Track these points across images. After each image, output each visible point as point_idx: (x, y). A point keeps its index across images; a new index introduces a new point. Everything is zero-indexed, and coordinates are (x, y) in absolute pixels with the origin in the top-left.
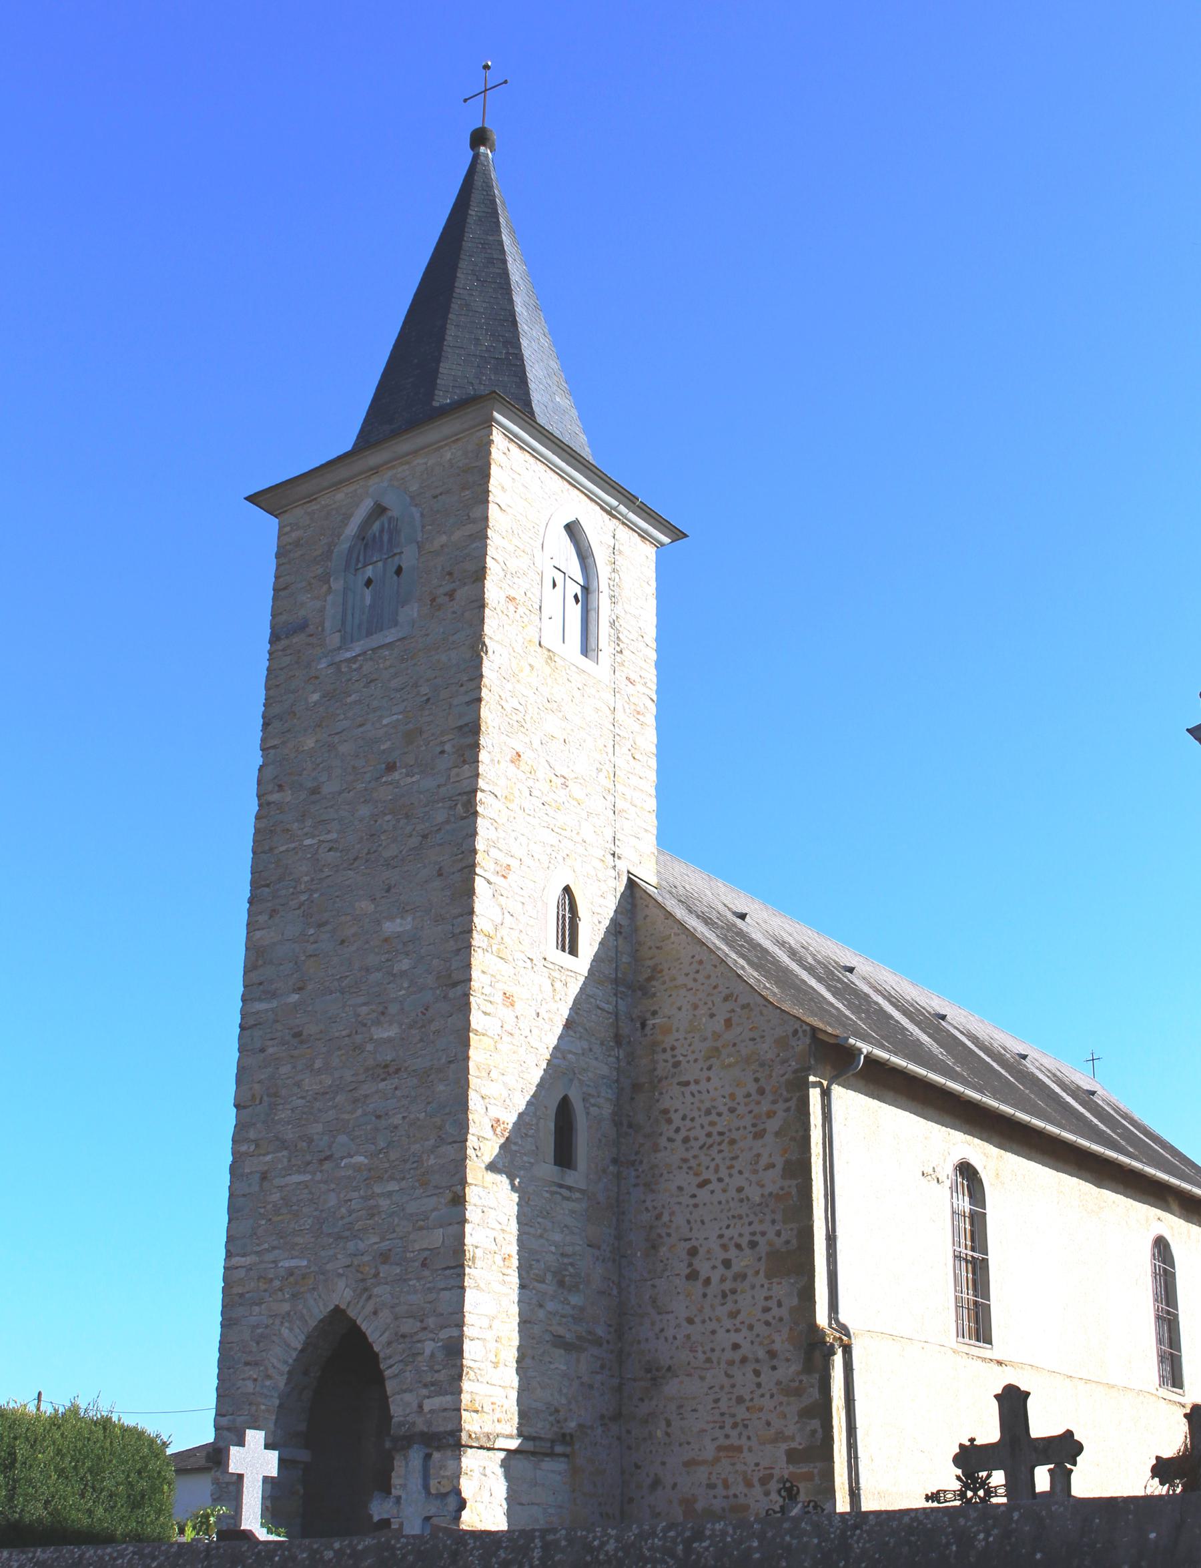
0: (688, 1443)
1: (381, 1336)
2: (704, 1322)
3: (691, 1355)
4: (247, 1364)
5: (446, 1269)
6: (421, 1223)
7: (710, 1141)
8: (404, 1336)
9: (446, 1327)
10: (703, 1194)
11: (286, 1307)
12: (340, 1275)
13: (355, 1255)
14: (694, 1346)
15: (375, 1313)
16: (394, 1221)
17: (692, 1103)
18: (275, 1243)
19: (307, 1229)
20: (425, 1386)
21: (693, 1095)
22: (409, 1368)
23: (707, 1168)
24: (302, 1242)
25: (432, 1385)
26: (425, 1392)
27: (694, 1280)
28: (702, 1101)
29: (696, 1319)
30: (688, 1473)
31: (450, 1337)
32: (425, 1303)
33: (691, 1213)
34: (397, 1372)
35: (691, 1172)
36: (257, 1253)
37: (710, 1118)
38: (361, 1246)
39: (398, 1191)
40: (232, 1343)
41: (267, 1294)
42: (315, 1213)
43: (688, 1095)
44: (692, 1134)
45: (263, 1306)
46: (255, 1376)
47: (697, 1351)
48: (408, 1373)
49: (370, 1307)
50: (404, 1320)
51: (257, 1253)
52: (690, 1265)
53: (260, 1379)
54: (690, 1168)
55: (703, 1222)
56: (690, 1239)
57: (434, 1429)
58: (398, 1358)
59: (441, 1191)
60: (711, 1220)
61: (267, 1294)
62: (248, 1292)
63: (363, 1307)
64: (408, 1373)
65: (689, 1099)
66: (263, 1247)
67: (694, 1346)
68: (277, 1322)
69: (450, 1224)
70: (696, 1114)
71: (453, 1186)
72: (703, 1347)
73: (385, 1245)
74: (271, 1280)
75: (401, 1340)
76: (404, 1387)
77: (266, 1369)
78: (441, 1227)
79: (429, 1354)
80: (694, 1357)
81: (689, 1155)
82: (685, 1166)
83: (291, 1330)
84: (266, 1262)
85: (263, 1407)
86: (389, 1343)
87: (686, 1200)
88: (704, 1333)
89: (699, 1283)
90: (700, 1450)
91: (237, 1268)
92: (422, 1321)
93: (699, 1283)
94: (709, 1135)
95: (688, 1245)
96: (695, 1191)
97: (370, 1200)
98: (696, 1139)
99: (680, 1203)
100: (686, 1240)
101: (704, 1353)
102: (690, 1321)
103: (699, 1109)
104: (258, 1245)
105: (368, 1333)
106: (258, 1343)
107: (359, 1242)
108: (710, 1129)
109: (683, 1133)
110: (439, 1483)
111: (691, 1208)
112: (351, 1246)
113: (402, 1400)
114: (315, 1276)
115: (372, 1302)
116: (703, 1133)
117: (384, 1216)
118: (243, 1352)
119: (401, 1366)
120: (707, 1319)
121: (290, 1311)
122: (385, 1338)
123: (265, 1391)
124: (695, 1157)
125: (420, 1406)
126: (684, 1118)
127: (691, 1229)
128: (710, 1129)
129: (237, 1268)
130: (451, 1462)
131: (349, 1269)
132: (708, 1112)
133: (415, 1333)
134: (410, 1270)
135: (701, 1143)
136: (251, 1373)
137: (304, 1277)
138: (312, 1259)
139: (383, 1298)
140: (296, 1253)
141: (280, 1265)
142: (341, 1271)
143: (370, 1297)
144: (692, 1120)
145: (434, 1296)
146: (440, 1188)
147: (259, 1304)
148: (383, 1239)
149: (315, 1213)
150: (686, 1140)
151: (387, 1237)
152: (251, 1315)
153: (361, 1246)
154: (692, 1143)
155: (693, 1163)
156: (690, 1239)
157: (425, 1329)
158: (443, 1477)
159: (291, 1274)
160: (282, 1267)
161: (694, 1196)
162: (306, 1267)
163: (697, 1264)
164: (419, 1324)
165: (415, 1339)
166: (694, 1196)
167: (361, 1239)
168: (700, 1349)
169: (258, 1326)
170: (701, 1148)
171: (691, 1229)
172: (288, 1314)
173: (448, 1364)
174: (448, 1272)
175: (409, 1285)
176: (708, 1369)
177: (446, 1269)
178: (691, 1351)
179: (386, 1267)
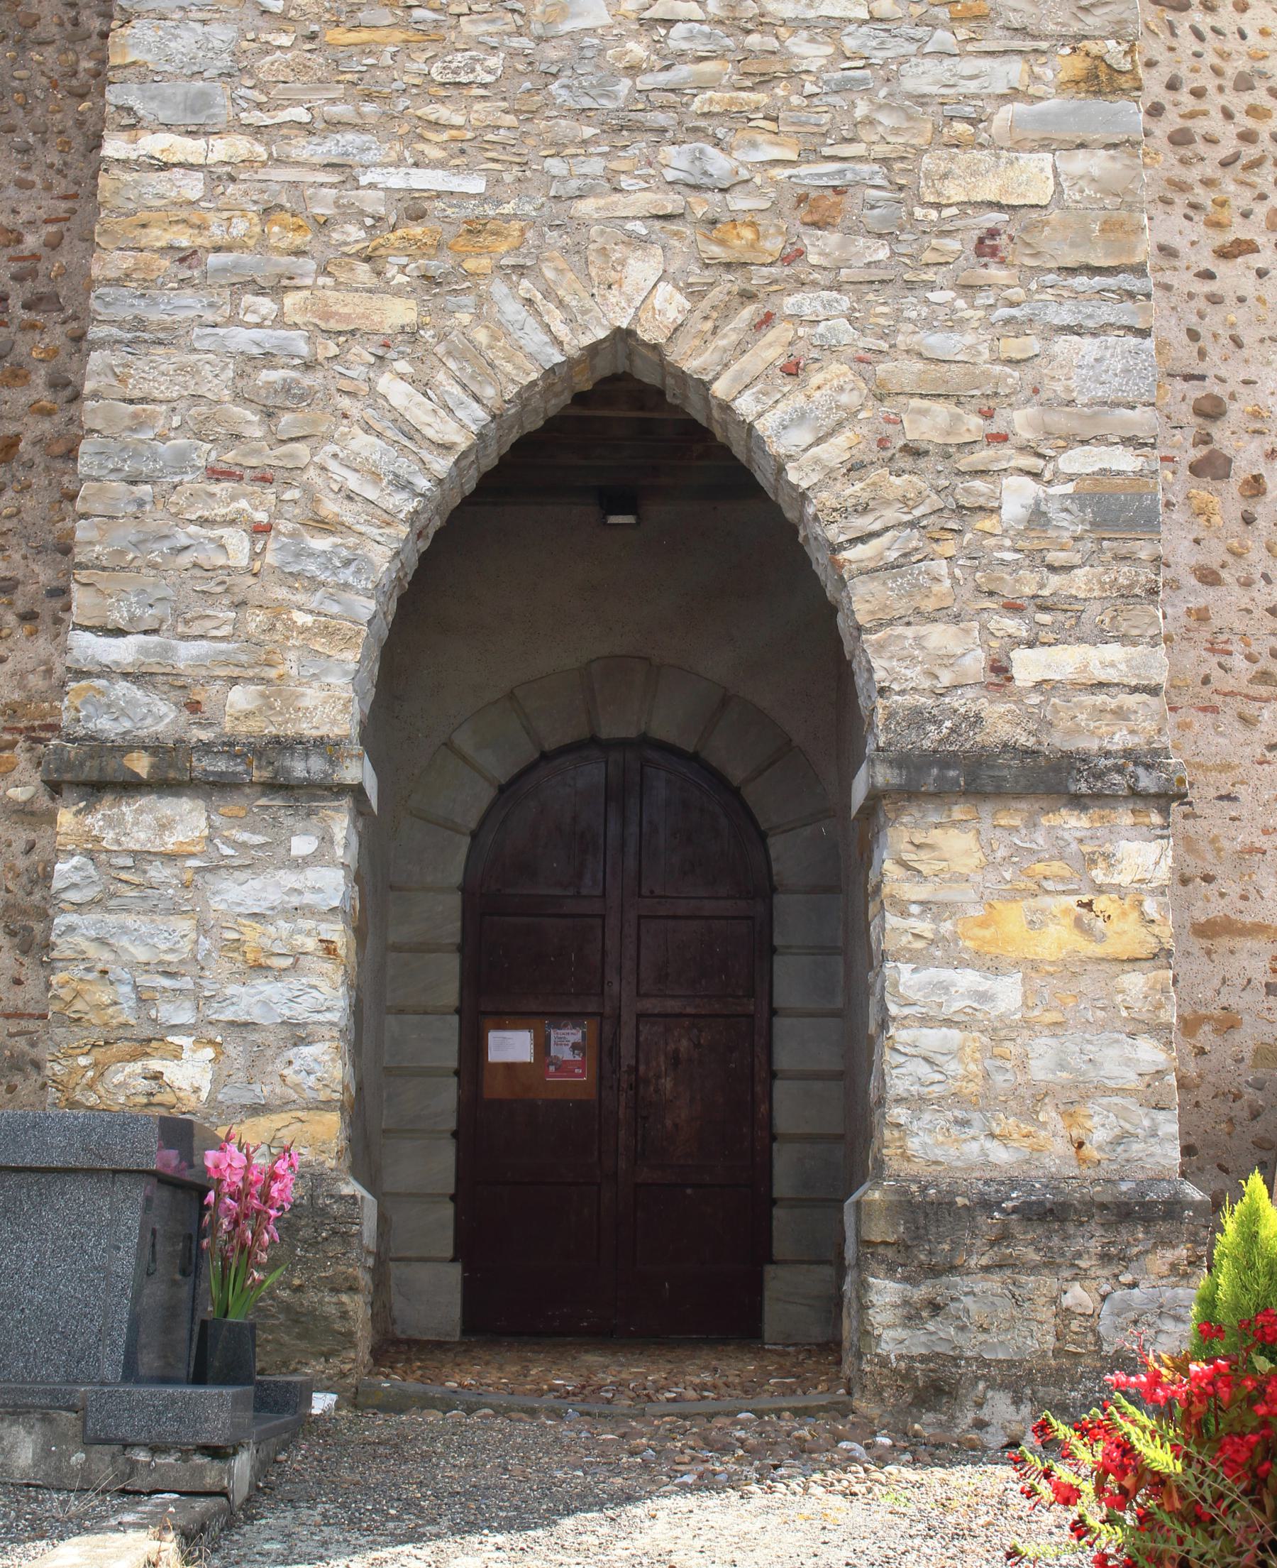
0: (1208, 879)
1: (819, 441)
2: (1247, 584)
3: (1214, 660)
4: (216, 474)
5: (1072, 271)
6: (961, 127)
7: (1250, 152)
8: (914, 451)
9: (1084, 442)
10: (1234, 276)
11: (401, 312)
12: (641, 242)
13: (696, 187)
14: (1222, 638)
15: (792, 370)
16: (853, 105)
17: (1197, 55)
18: (341, 111)
19: (484, 86)
20: (1013, 608)
21: (1199, 36)
22: (949, 548)
23: (1246, 215)
24: (458, 120)
25: (1044, 608)
26: (1012, 625)
27: (1215, 478)
28: (1224, 55)
29: (1224, 574)
30: (1209, 953)
31: (1103, 472)
32: (994, 361)
33: (1201, 316)
34: (892, 555)
35: (1199, 217)
36: (257, 131)
37: (1248, 98)
38: (719, 164)
39: (865, 22)
40: (143, 400)
41: (310, 265)
42: (516, 42)
43: (1183, 30)
44: (1199, 126)
45: (290, 300)
46: (261, 517)
47: (1230, 653)
48: (941, 567)
49: (770, 349)
50: (915, 403)
51: (257, 131)
52: (1205, 439)
53: (284, 526)
54: (1194, 206)
55: (1237, 343)
56: (1202, 378)
57: (1058, 741)
58: (892, 515)
59: (1044, 45)
60: (1262, 341)
61: (310, 265)
62: (218, 249)
63: (741, 348)
64: (941, 567)
65: (1188, 43)
66: (283, 116)
67: (1222, 638)
68: (361, 353)
69: (1082, 146)
70: (1210, 83)
71: (1085, 37)
72: (1248, 645)
73: (814, 173)
74: (324, 224)
75: (905, 462)
76: (929, 605)
77: (312, 498)
78: (1045, 145)
79: (1021, 513)
80: (1220, 665)
81: (1193, 174)
82: (1180, 200)
83: (424, 386)
84: (297, 164)
85: (302, 619)
86: (855, 468)
87: (1183, 281)
88: (1249, 611)
89: (1233, 486)
90: (1244, 898)
91: (166, 166)
92: (988, 415)
93: (1233, 486)
94: (1248, 137)
95: (1195, 391)
96: (1208, 262)
97: (749, 32)
98: (1211, 140)
99: (1167, 288)
100: (1188, 378)
101: (1250, 658)
102: (1209, 577)
103: (1217, 72)
104: (259, 106)
105: (765, 426)
106: (269, 414)
107: (711, 151)
108: (1250, 123)
109: (1172, 121)
110: (1088, 905)
111: (1201, 303)
112: (676, 159)
113: (918, 639)
114: (522, 231)
115: (780, 333)
116: (1231, 130)
117: (810, 88)
118: (199, 436)
119: (914, 539)
120: (1257, 576)
121: (421, 326)
122: (836, 450)
123: (312, 567)
124: (1208, 183)
125: (1000, 669)
126: (1173, 85)
127: (1202, 354)
128: (1250, 123)
129: (166, 166)
130: (1135, 845)
131: (672, 226)
132: (1244, 83)
133: (960, 446)
134: (928, 257)
135: (1225, 151)
136: (243, 504)
137: (475, 228)
138: (508, 178)
139: (821, 328)
140: (435, 153)
141: (364, 180)
142: (639, 228)
143: (767, 320)
144: (1198, 93)
145: (1032, 345)
146: (1034, 37)
147: (278, 288)
148: (810, 154)
149: (516, 42)
150: (1180, 139)
151: (827, 151)
152: (232, 321)
153: (719, 164)
154: (1201, 147)
155: (1203, 196)
156: (1202, 378)
157: (1001, 438)
158: (1100, 890)
159: (418, 216)
160: (372, 186)
161: (1208, 275)
162: (482, 198)
163: (1224, 437)
164: (975, 421)
165: (964, 463)
166: (1208, 275)
167: (717, 143)
168: (1237, 647)
169: (268, 359)
170: (1225, 164)
171: (1202, 354)
172: (412, 334)
173: (1101, 550)
174: (1081, 282)
175: (927, 302)
176: (1267, 700)
177: (1072, 271)
178: (1212, 650)
179: (831, 239)
